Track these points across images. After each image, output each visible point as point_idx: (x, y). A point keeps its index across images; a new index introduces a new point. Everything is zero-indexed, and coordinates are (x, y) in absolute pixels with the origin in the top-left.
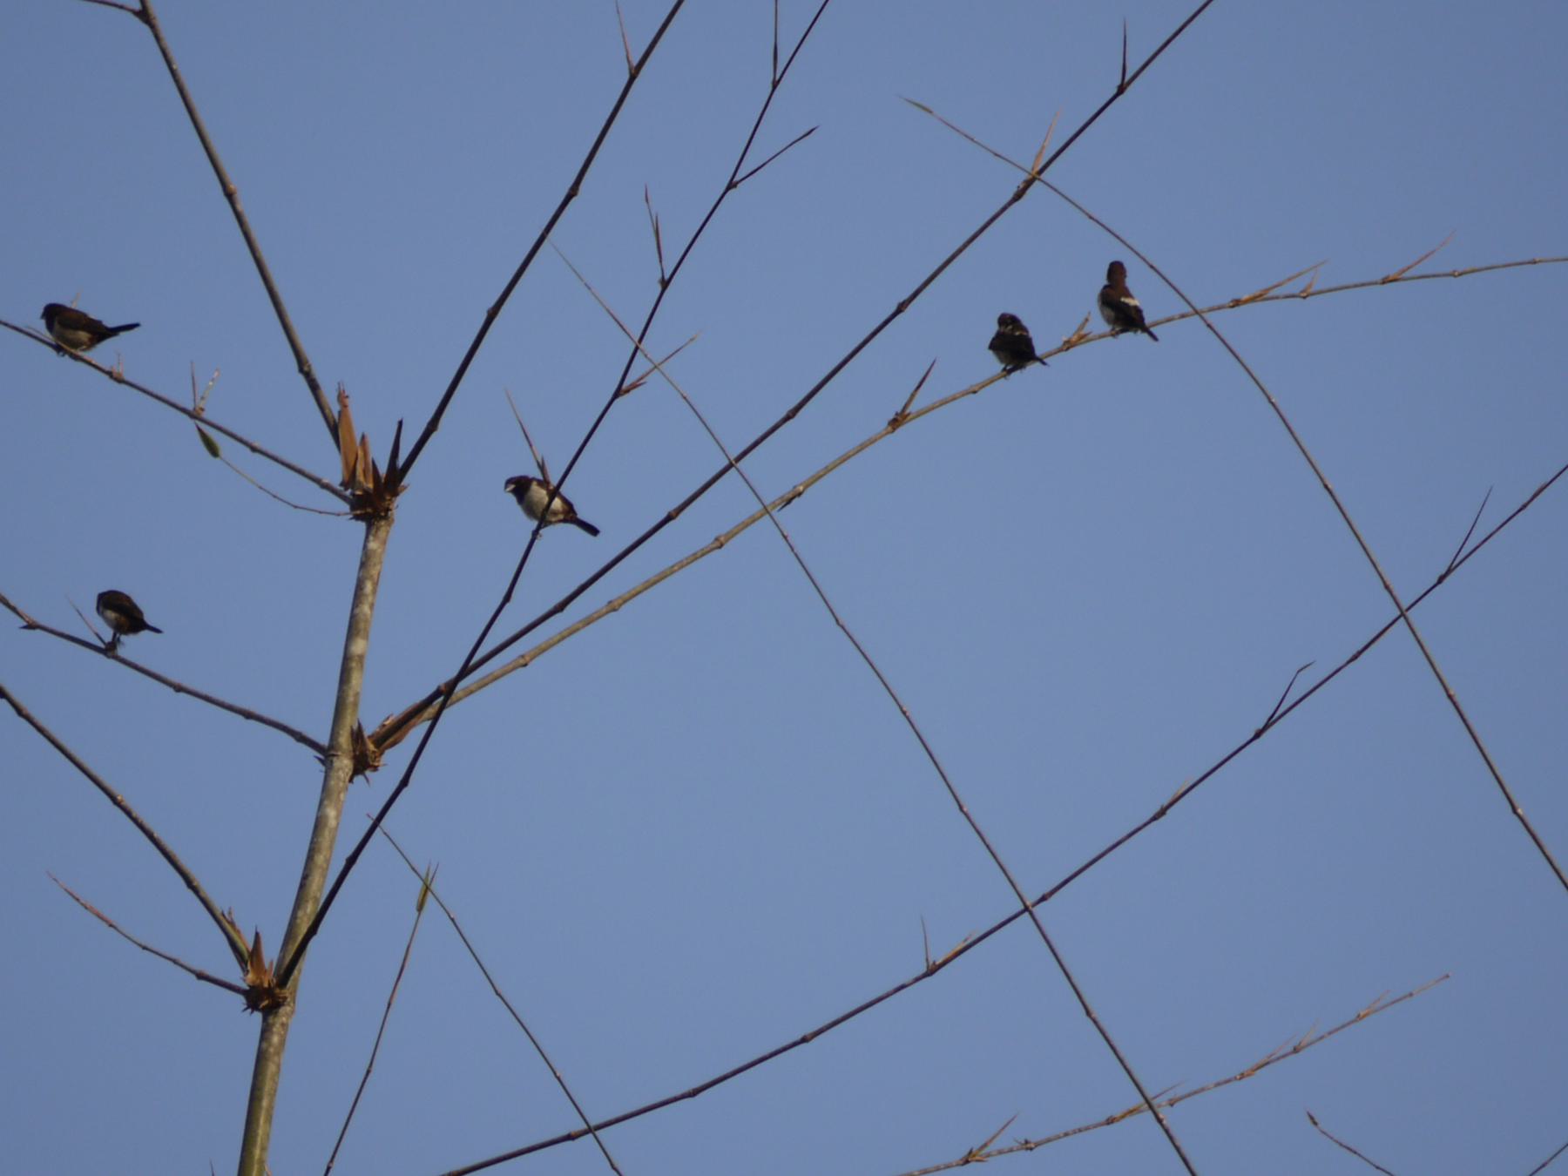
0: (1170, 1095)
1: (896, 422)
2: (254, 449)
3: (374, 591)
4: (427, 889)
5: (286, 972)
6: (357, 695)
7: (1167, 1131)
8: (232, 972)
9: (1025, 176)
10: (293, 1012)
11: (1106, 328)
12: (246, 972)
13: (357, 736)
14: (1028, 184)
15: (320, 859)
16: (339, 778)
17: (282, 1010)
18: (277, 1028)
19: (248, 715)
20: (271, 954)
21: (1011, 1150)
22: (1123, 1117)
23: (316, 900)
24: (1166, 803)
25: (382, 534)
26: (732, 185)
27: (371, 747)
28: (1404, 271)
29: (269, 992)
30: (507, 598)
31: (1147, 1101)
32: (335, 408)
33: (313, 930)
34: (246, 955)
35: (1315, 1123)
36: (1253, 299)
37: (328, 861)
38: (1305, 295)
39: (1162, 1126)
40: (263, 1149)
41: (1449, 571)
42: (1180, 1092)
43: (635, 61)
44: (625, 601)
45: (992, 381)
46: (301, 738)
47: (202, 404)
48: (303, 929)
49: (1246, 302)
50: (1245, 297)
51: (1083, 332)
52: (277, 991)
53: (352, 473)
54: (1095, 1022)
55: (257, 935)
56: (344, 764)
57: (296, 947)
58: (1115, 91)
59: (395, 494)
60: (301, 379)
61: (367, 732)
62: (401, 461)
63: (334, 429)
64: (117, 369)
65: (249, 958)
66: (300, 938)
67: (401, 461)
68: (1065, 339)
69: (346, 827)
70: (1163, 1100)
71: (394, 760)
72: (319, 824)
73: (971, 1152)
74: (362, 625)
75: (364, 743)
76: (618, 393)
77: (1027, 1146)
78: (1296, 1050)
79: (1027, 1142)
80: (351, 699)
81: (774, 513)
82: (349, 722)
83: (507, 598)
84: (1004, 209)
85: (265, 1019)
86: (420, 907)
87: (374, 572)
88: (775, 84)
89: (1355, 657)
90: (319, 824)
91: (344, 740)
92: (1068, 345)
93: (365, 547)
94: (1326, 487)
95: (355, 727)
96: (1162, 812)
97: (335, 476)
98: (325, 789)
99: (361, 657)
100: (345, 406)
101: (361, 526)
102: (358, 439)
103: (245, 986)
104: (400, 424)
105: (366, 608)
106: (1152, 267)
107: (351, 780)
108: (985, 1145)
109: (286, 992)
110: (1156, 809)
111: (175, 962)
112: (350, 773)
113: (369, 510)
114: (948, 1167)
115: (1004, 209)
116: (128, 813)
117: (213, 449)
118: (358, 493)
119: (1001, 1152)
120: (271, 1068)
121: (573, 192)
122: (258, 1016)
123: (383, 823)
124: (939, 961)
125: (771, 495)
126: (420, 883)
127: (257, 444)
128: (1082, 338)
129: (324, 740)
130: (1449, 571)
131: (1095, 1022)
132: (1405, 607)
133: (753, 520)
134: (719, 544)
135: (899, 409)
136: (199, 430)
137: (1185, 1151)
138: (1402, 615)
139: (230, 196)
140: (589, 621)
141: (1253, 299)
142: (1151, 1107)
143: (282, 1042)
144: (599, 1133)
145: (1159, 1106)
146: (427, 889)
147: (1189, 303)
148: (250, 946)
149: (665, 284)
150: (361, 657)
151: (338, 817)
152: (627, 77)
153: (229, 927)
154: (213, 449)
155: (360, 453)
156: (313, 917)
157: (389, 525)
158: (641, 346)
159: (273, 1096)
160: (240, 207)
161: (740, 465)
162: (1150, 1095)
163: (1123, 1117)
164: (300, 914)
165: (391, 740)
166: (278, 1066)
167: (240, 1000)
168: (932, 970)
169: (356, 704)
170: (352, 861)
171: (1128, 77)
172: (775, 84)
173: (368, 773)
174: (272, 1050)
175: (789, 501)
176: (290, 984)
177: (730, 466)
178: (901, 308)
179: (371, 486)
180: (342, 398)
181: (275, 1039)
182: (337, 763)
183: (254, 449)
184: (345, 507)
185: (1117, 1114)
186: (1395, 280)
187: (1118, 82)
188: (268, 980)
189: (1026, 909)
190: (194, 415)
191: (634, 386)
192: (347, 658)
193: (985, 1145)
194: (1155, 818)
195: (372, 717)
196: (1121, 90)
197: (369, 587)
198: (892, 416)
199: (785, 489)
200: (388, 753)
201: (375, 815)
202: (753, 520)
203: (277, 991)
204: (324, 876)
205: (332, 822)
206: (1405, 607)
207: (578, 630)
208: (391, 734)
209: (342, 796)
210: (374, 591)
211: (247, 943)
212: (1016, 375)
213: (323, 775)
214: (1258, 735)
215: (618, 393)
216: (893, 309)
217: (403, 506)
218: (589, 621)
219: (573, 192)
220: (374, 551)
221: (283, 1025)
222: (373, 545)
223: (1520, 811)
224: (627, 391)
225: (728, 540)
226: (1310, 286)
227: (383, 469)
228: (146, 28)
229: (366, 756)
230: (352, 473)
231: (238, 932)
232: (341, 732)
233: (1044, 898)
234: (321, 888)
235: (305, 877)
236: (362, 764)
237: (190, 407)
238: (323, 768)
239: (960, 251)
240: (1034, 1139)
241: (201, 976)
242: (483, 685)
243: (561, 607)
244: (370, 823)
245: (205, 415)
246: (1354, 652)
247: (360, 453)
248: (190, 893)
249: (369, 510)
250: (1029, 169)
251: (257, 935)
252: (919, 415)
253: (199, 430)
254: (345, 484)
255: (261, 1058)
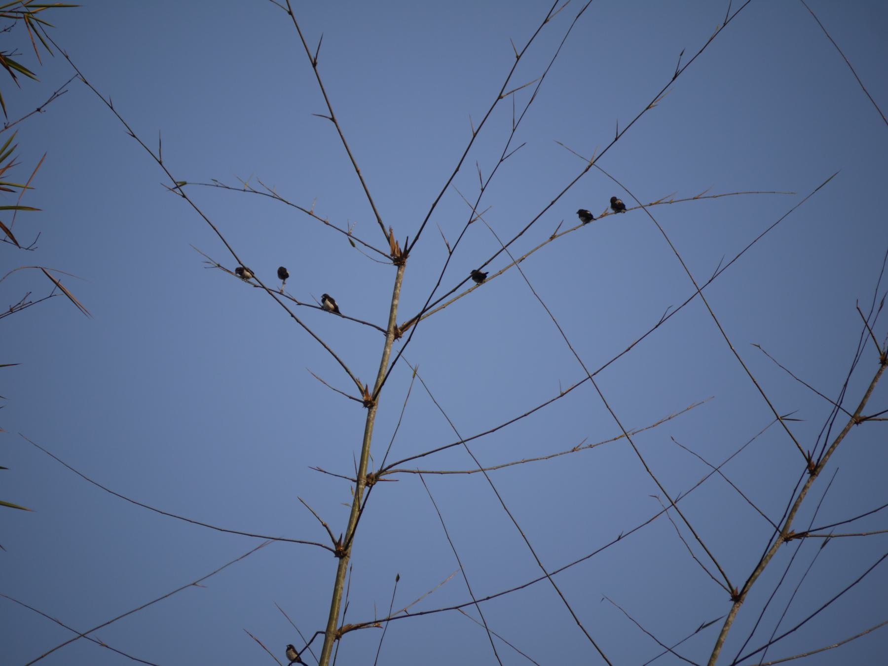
0: (633, 431)
1: (552, 238)
2: (365, 245)
3: (400, 286)
4: (415, 373)
5: (375, 396)
6: (395, 316)
7: (630, 441)
8: (359, 396)
9: (589, 164)
10: (377, 408)
11: (614, 211)
12: (363, 396)
13: (396, 328)
14: (590, 167)
15: (385, 364)
16: (390, 340)
17: (374, 407)
18: (372, 412)
19: (364, 323)
20: (371, 391)
21: (586, 448)
22: (619, 438)
23: (384, 375)
24: (630, 346)
25: (402, 269)
26: (502, 160)
27: (400, 331)
28: (699, 196)
29: (370, 402)
30: (438, 284)
31: (626, 434)
32: (389, 233)
33: (383, 384)
34: (363, 391)
35: (673, 439)
36: (656, 203)
37: (387, 364)
38: (671, 202)
39: (629, 439)
40: (369, 447)
41: (712, 279)
42: (636, 431)
43: (475, 132)
44: (473, 289)
45: (580, 226)
46: (379, 329)
47: (351, 231)
48: (380, 384)
49: (653, 204)
50: (653, 203)
51: (606, 212)
52: (373, 402)
53: (394, 252)
54: (609, 409)
55: (367, 386)
56: (392, 336)
57: (378, 389)
58: (614, 140)
59: (406, 258)
60: (379, 224)
61: (398, 327)
62: (408, 248)
63: (388, 239)
64: (328, 221)
65: (364, 392)
66: (349, 537)
67: (408, 248)
68: (601, 214)
69: (392, 355)
70: (631, 433)
71: (406, 335)
72: (385, 354)
73: (574, 448)
74: (397, 296)
75: (397, 330)
76: (470, 223)
77: (591, 446)
78: (669, 419)
79: (591, 445)
80: (394, 317)
81: (517, 263)
82: (393, 324)
83: (438, 284)
84: (582, 174)
85: (369, 410)
86: (414, 377)
87: (400, 280)
88: (514, 130)
89: (685, 304)
90: (385, 354)
91: (392, 329)
92: (602, 216)
93: (398, 273)
94: (677, 254)
95: (395, 325)
96: (629, 349)
97: (389, 253)
98: (386, 343)
99: (396, 305)
100: (391, 232)
101: (396, 267)
102: (395, 243)
103: (363, 400)
104: (408, 237)
105: (398, 291)
106: (626, 190)
107: (394, 341)
108: (579, 446)
109: (375, 402)
110: (627, 348)
111: (343, 393)
112: (393, 338)
113: (399, 263)
114: (568, 452)
115: (582, 174)
116: (329, 350)
117: (353, 245)
118: (396, 257)
119: (583, 448)
120: (371, 424)
121: (457, 170)
122: (367, 409)
123: (402, 354)
124: (564, 392)
125: (516, 258)
126: (413, 372)
127: (367, 244)
128: (606, 214)
129: (386, 329)
130: (712, 279)
131: (609, 409)
132: (700, 289)
133: (511, 266)
134: (501, 273)
135: (553, 234)
136: (349, 239)
137: (636, 447)
138: (699, 291)
139: (358, 172)
140: (463, 295)
141: (656, 203)
142: (627, 436)
143: (374, 417)
144: (465, 443)
145: (629, 435)
146: (415, 373)
147: (645, 210)
148: (365, 389)
149: (483, 190)
150: (396, 305)
151: (390, 351)
152: (472, 136)
153: (358, 383)
154: (353, 245)
155: (396, 246)
156: (383, 380)
157: (404, 267)
158: (475, 211)
159: (371, 432)
160: (361, 175)
161: (507, 248)
162: (626, 432)
163: (619, 438)
164: (379, 379)
165: (405, 329)
166: (373, 423)
167: (362, 404)
168: (562, 395)
169: (395, 319)
170: (394, 363)
171: (618, 136)
172: (514, 130)
173: (398, 338)
174: (371, 419)
175: (521, 261)
176: (376, 400)
177: (504, 249)
178: (552, 203)
179: (399, 255)
180: (391, 230)
181: (372, 416)
182: (390, 336)
183: (365, 245)
184: (392, 262)
185: (617, 437)
186: (697, 198)
187: (615, 137)
188: (370, 399)
189: (590, 377)
190: (348, 235)
191: (474, 220)
192: (392, 305)
193: (579, 446)
194: (627, 351)
195: (400, 322)
196: (616, 139)
197: (399, 285)
198: (551, 236)
199: (519, 257)
200: (404, 333)
201: (399, 351)
202: (511, 266)
203: (373, 402)
204: (386, 369)
205: (388, 353)
206: (700, 289)
207: (459, 297)
208: (405, 328)
209: (391, 345)
210: (400, 286)
211: (364, 388)
212: (587, 225)
213: (385, 340)
214: (657, 327)
215: (470, 223)
216: (550, 203)
217: (408, 261)
218: (463, 295)
219: (457, 170)
220: (400, 274)
221: (375, 412)
222: (400, 273)
223: (733, 348)
224: (472, 222)
225: (503, 272)
226: (672, 200)
227: (403, 251)
228: (333, 123)
229: (398, 334)
230: (394, 252)
231: (361, 384)
232: (361, 479)
233: (595, 374)
234: (385, 371)
235: (381, 369)
236: (397, 336)
237: (347, 232)
238: (385, 337)
239: (569, 187)
240: (593, 444)
241: (350, 398)
242: (432, 313)
243: (454, 290)
244: (398, 354)
245: (351, 235)
246: (685, 302)
247: (396, 246)
248: (347, 373)
249: (399, 263)
250: (590, 160)
251: (367, 386)
252: (559, 236)
253: (349, 239)
254: (392, 255)
255: (368, 421)
